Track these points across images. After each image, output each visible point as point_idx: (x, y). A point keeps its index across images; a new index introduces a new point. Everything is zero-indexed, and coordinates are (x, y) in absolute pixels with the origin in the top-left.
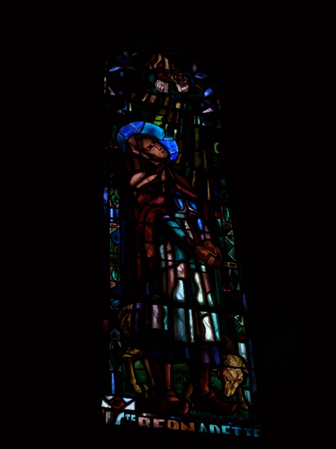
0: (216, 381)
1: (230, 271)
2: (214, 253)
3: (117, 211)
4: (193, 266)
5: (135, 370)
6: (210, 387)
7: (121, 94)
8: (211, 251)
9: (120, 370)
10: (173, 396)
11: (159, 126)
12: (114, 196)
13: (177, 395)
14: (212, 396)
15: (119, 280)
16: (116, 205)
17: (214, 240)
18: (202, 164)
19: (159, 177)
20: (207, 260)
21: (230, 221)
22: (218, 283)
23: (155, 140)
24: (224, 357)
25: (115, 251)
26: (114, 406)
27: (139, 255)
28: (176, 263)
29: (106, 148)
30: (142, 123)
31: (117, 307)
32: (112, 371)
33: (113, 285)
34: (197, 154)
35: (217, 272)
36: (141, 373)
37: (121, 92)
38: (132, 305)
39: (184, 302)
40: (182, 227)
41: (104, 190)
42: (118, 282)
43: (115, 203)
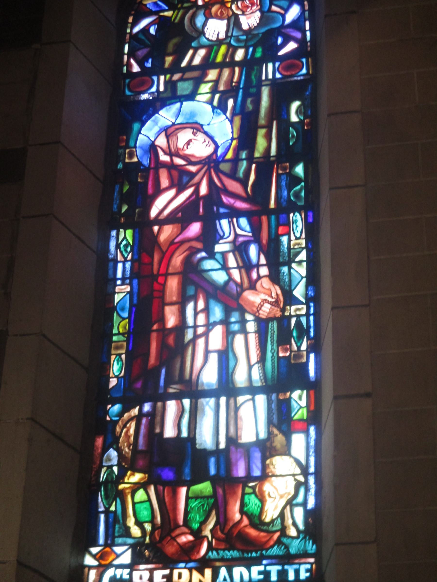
0: (252, 502)
1: (293, 320)
2: (272, 297)
3: (128, 265)
4: (236, 327)
5: (134, 504)
6: (242, 512)
7: (288, 164)
8: (265, 294)
9: (113, 508)
10: (184, 534)
11: (204, 102)
12: (124, 243)
13: (192, 532)
14: (243, 524)
15: (122, 374)
16: (126, 255)
17: (275, 277)
18: (268, 149)
19: (197, 191)
20: (258, 311)
21: (303, 236)
22: (272, 346)
23: (197, 128)
24: (264, 384)
25: (121, 331)
26: (101, 561)
27: (155, 327)
28: (209, 326)
29: (120, 166)
30: (178, 105)
31: (116, 416)
32: (102, 512)
33: (113, 382)
34: (262, 132)
35: (274, 326)
36: (142, 508)
37: (150, 61)
38: (137, 408)
39: (195, 530)
40: (225, 267)
41: (110, 235)
42: (122, 377)
43: (124, 253)
